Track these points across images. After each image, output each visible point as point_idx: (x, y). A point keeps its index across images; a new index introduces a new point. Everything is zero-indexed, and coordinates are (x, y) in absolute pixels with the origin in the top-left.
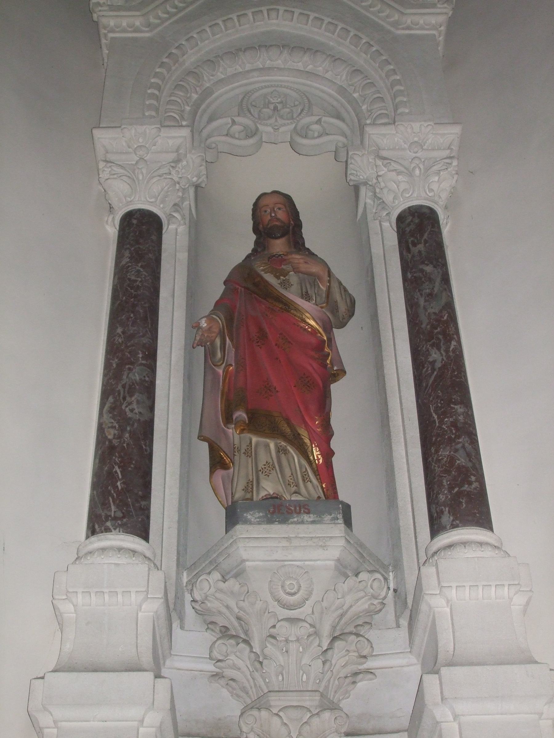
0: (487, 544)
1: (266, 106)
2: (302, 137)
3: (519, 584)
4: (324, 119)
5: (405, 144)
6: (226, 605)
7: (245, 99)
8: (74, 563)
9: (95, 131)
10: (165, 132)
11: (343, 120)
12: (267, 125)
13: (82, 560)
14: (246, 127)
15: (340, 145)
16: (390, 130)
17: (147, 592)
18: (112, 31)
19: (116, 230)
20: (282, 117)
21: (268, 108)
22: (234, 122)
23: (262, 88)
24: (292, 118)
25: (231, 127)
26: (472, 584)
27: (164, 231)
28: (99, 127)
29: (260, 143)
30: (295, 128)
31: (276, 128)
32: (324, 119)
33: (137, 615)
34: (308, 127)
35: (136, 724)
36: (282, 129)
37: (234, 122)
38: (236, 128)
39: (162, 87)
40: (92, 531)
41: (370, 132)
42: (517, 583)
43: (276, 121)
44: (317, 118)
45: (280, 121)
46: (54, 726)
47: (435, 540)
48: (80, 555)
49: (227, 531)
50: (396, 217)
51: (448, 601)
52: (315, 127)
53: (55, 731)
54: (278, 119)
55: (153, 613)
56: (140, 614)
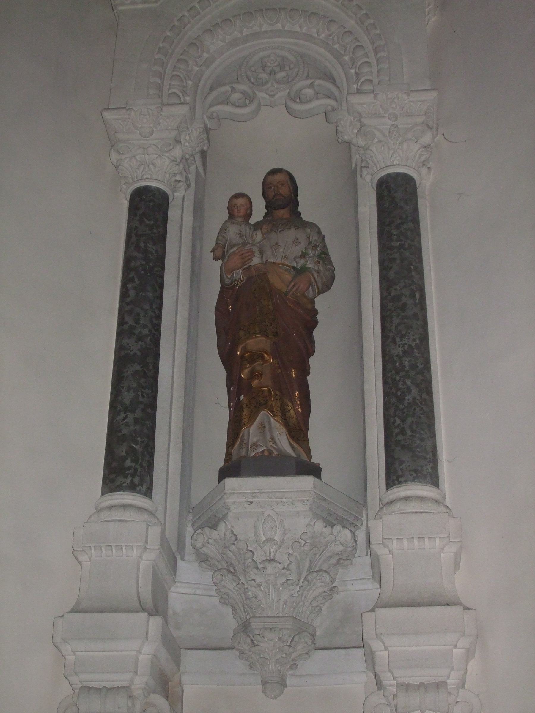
14: (244, 93)
15: (330, 108)
22: (233, 89)
29: (259, 107)
30: (289, 94)
31: (272, 93)
32: (318, 82)
35: (134, 653)
37: (233, 89)
38: (236, 96)
43: (272, 86)
46: (73, 654)
49: (220, 481)
53: (74, 657)
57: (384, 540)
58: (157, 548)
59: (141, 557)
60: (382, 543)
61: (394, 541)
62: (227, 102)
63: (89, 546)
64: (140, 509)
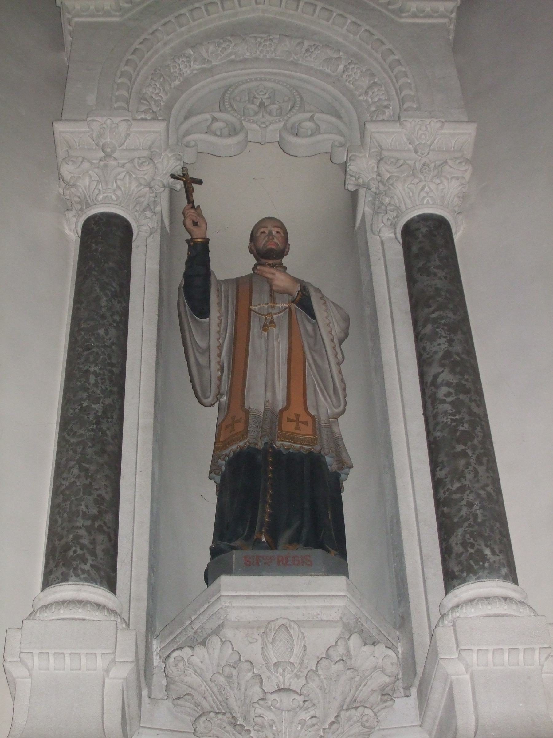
0: (511, 599)
1: (252, 101)
2: (293, 134)
3: (550, 647)
4: (317, 115)
5: (410, 143)
6: (508, 601)
7: (228, 92)
8: (28, 618)
9: (56, 125)
10: (137, 127)
11: (339, 117)
12: (254, 122)
13: (38, 615)
16: (395, 128)
17: (114, 653)
18: (78, 16)
19: (78, 238)
20: (270, 114)
21: (253, 103)
23: (246, 82)
24: (281, 114)
25: (211, 124)
26: (495, 648)
27: (134, 238)
28: (61, 120)
29: (246, 141)
32: (317, 115)
33: (104, 682)
34: (299, 125)
36: (271, 127)
38: (217, 125)
39: (134, 77)
40: (46, 583)
41: (372, 130)
42: (548, 646)
43: (263, 116)
44: (310, 115)
45: (268, 117)
47: (450, 595)
48: (36, 609)
50: (404, 223)
51: (467, 667)
52: (309, 124)
54: (265, 115)
55: (122, 680)
56: (107, 680)
57: (22, 655)
58: (131, 660)
59: (107, 671)
60: (382, 669)
61: (51, 657)
62: (209, 131)
63: (47, 653)
64: (99, 607)
